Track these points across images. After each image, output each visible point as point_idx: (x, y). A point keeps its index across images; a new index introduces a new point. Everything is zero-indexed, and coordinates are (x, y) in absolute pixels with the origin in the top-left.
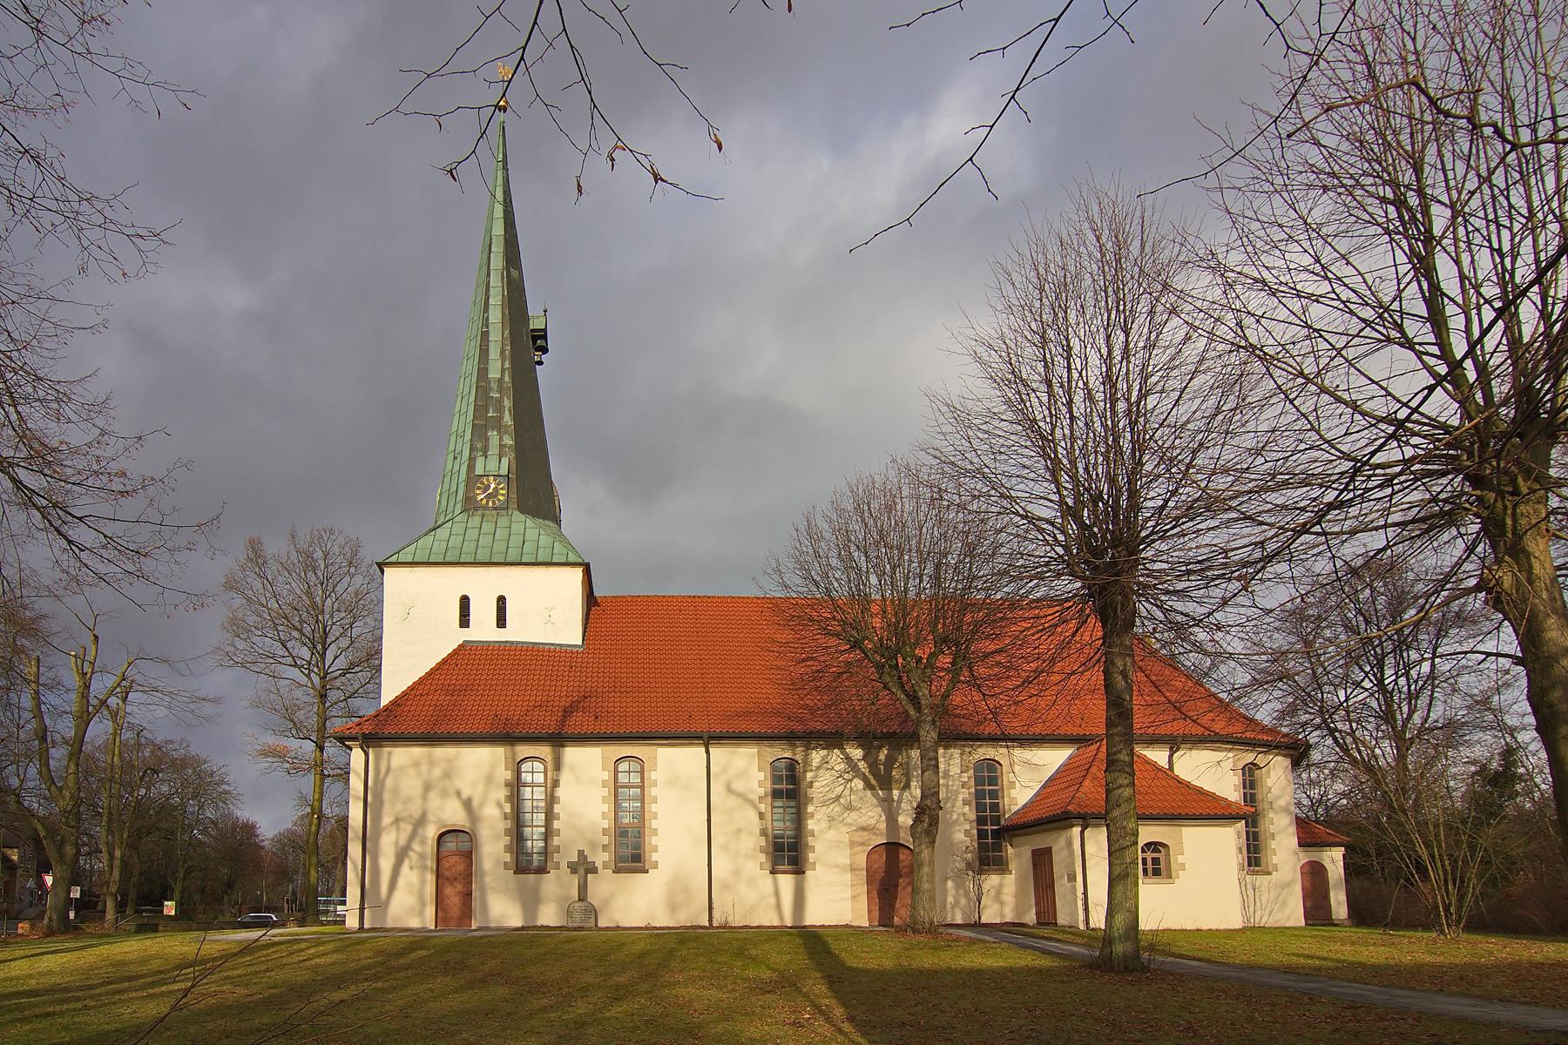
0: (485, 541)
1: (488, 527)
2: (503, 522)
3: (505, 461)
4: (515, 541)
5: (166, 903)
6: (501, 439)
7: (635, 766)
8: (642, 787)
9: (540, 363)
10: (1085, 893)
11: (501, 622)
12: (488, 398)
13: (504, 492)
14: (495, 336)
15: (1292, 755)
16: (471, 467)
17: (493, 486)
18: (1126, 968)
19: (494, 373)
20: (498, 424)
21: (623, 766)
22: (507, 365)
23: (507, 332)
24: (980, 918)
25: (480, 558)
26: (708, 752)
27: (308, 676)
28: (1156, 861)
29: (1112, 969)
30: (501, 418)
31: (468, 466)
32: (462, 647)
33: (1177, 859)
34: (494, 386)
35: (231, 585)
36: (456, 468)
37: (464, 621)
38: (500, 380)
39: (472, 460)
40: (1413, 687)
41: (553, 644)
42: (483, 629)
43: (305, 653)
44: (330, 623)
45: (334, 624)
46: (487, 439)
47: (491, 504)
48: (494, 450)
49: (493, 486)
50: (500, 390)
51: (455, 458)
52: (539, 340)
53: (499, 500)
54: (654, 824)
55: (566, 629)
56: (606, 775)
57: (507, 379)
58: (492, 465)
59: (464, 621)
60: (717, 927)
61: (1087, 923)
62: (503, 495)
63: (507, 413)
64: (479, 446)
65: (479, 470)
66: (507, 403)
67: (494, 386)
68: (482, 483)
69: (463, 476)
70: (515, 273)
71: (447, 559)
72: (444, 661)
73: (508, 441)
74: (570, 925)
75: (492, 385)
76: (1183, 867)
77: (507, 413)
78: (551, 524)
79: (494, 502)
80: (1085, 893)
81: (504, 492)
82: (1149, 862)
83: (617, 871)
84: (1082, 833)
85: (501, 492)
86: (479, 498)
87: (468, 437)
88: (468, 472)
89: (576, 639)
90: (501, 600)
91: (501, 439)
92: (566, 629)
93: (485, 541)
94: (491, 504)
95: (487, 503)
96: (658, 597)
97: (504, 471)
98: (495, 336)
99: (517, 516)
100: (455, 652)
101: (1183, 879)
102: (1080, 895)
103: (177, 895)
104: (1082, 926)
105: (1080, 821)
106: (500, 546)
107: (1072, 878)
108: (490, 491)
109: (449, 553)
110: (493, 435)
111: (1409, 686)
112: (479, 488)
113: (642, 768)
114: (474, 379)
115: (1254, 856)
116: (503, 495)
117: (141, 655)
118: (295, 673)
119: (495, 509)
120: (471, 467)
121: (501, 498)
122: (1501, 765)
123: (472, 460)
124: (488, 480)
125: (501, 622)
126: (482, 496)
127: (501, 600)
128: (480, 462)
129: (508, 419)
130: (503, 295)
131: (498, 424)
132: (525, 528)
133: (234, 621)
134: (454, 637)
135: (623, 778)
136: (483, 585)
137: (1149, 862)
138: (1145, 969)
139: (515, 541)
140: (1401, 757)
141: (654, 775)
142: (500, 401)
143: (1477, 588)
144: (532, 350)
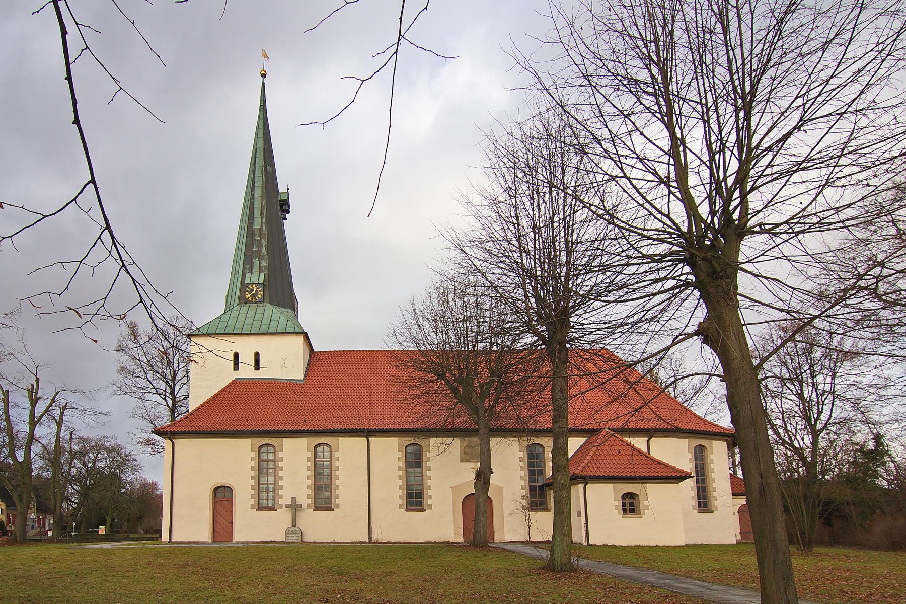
0: (249, 321)
1: (251, 313)
2: (260, 310)
3: (262, 275)
4: (266, 321)
5: (100, 527)
6: (260, 263)
7: (326, 449)
8: (330, 461)
9: (286, 219)
10: (587, 523)
11: (257, 367)
12: (253, 239)
13: (261, 293)
14: (258, 205)
15: (727, 440)
16: (243, 279)
17: (255, 289)
18: (561, 569)
19: (257, 226)
20: (259, 255)
21: (320, 449)
22: (264, 221)
23: (264, 202)
24: (530, 538)
25: (245, 331)
26: (368, 441)
27: (165, 399)
28: (632, 504)
29: (553, 570)
30: (260, 251)
31: (242, 279)
32: (234, 381)
33: (643, 503)
34: (257, 232)
35: (122, 349)
36: (236, 280)
37: (236, 368)
38: (260, 229)
39: (244, 276)
40: (820, 398)
41: (286, 379)
42: (247, 372)
43: (163, 385)
44: (177, 369)
45: (179, 370)
46: (252, 263)
47: (254, 300)
48: (256, 269)
49: (255, 289)
50: (260, 235)
51: (235, 275)
52: (284, 206)
53: (259, 298)
54: (337, 482)
56: (310, 454)
57: (264, 228)
58: (255, 278)
59: (236, 368)
60: (374, 542)
61: (588, 541)
62: (260, 295)
63: (264, 248)
64: (248, 267)
65: (247, 281)
66: (264, 242)
67: (257, 232)
68: (249, 288)
69: (239, 284)
70: (269, 168)
71: (226, 332)
72: (223, 390)
73: (264, 264)
74: (287, 540)
75: (256, 232)
76: (647, 508)
77: (264, 248)
78: (290, 311)
79: (255, 299)
80: (587, 523)
81: (261, 293)
82: (627, 505)
83: (316, 509)
84: (585, 487)
85: (260, 293)
86: (247, 297)
87: (242, 262)
88: (241, 283)
89: (300, 376)
90: (257, 355)
91: (260, 263)
93: (249, 321)
94: (254, 300)
95: (252, 299)
96: (366, 351)
97: (261, 281)
98: (258, 205)
99: (269, 306)
100: (230, 385)
101: (647, 515)
102: (583, 526)
103: (108, 523)
104: (585, 543)
105: (583, 480)
106: (256, 324)
107: (579, 514)
108: (254, 292)
109: (227, 328)
110: (256, 261)
111: (818, 398)
112: (247, 291)
113: (331, 450)
114: (246, 230)
115: (704, 503)
116: (260, 295)
117: (64, 389)
118: (157, 398)
119: (256, 303)
120: (243, 279)
121: (260, 296)
122: (874, 446)
123: (244, 276)
124: (252, 287)
125: (257, 367)
126: (249, 296)
127: (257, 355)
128: (248, 276)
129: (264, 251)
130: (262, 181)
131: (259, 255)
132: (274, 314)
133: (123, 369)
134: (228, 376)
135: (320, 455)
136: (246, 347)
137: (627, 505)
138: (573, 569)
139: (266, 321)
140: (815, 442)
141: (337, 454)
142: (260, 241)
143: (697, 333)
144: (280, 212)
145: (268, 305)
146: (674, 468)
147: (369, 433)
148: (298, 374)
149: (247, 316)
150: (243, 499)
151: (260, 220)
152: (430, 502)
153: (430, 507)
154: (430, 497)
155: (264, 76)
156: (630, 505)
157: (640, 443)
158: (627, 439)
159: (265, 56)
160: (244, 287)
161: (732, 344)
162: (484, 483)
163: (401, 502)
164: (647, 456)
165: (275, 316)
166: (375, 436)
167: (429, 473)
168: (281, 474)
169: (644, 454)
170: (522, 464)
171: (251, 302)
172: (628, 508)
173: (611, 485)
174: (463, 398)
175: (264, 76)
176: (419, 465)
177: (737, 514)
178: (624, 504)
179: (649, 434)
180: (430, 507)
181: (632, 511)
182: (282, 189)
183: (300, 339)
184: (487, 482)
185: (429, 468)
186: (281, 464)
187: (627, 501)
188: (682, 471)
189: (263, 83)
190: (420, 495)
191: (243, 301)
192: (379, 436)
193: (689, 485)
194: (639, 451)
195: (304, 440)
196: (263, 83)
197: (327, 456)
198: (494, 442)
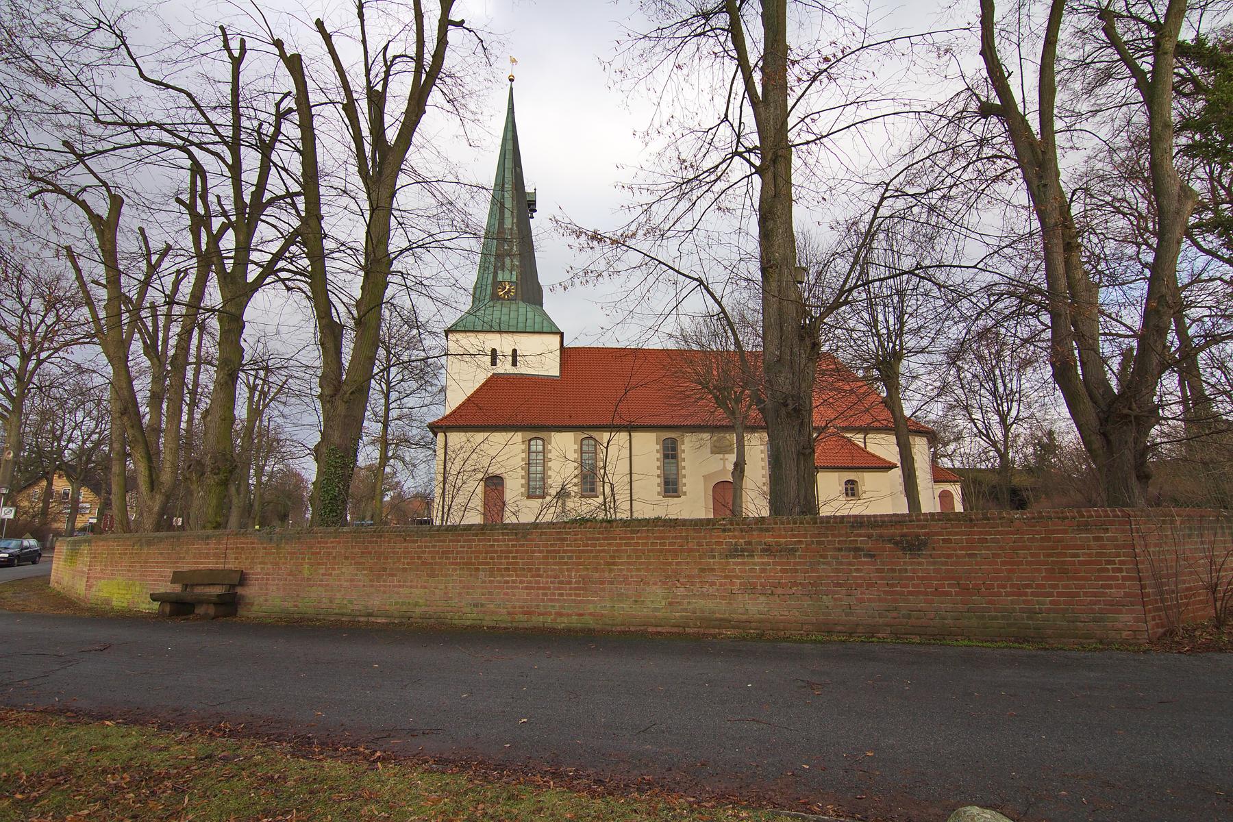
7: (540, 442)
11: (514, 363)
14: (508, 204)
17: (507, 287)
21: (585, 442)
22: (515, 221)
28: (852, 489)
33: (861, 488)
37: (494, 363)
38: (512, 229)
42: (504, 367)
49: (507, 287)
52: (531, 206)
55: (551, 367)
59: (494, 363)
65: (500, 278)
92: (551, 367)
106: (513, 322)
110: (508, 261)
125: (514, 363)
132: (524, 310)
136: (504, 344)
139: (521, 319)
145: (521, 303)
146: (884, 460)
147: (630, 428)
148: (555, 371)
149: (497, 313)
150: (514, 488)
151: (510, 220)
152: (684, 489)
153: (685, 493)
154: (685, 485)
155: (512, 80)
156: (851, 489)
157: (858, 439)
158: (849, 435)
159: (514, 61)
160: (497, 284)
161: (896, 409)
162: (741, 472)
163: (659, 489)
164: (864, 450)
165: (530, 315)
166: (635, 431)
167: (683, 464)
168: (550, 464)
169: (862, 449)
170: (763, 456)
171: (504, 299)
172: (849, 492)
173: (837, 474)
174: (721, 402)
175: (512, 80)
176: (674, 457)
177: (937, 499)
178: (846, 489)
179: (866, 430)
180: (685, 493)
181: (853, 495)
182: (529, 189)
183: (557, 338)
184: (743, 471)
185: (684, 460)
186: (549, 456)
187: (849, 486)
188: (890, 463)
189: (511, 89)
190: (676, 483)
191: (495, 297)
192: (646, 431)
193: (897, 472)
194: (858, 446)
195: (571, 434)
196: (511, 89)
197: (540, 448)
198: (747, 436)
